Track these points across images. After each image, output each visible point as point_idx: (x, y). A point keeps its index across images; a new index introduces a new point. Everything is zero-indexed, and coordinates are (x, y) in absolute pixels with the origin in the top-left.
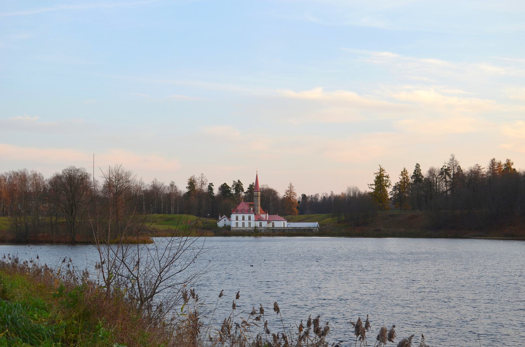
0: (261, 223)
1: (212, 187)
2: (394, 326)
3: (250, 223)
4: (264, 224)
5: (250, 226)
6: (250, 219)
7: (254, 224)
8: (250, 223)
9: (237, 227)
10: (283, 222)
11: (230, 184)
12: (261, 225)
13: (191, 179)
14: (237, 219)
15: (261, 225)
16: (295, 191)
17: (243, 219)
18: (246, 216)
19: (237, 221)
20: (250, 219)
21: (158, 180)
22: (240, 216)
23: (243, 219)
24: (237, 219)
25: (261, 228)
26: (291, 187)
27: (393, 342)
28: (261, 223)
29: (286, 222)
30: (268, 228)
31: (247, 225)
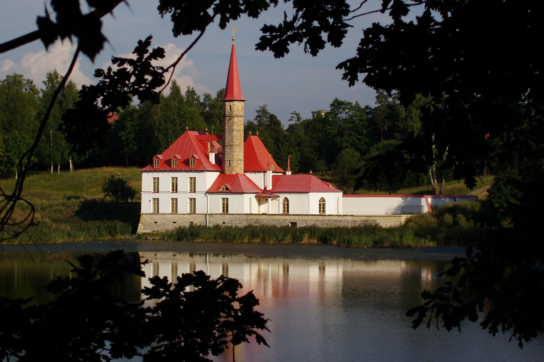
17: (175, 189)
23: (175, 189)
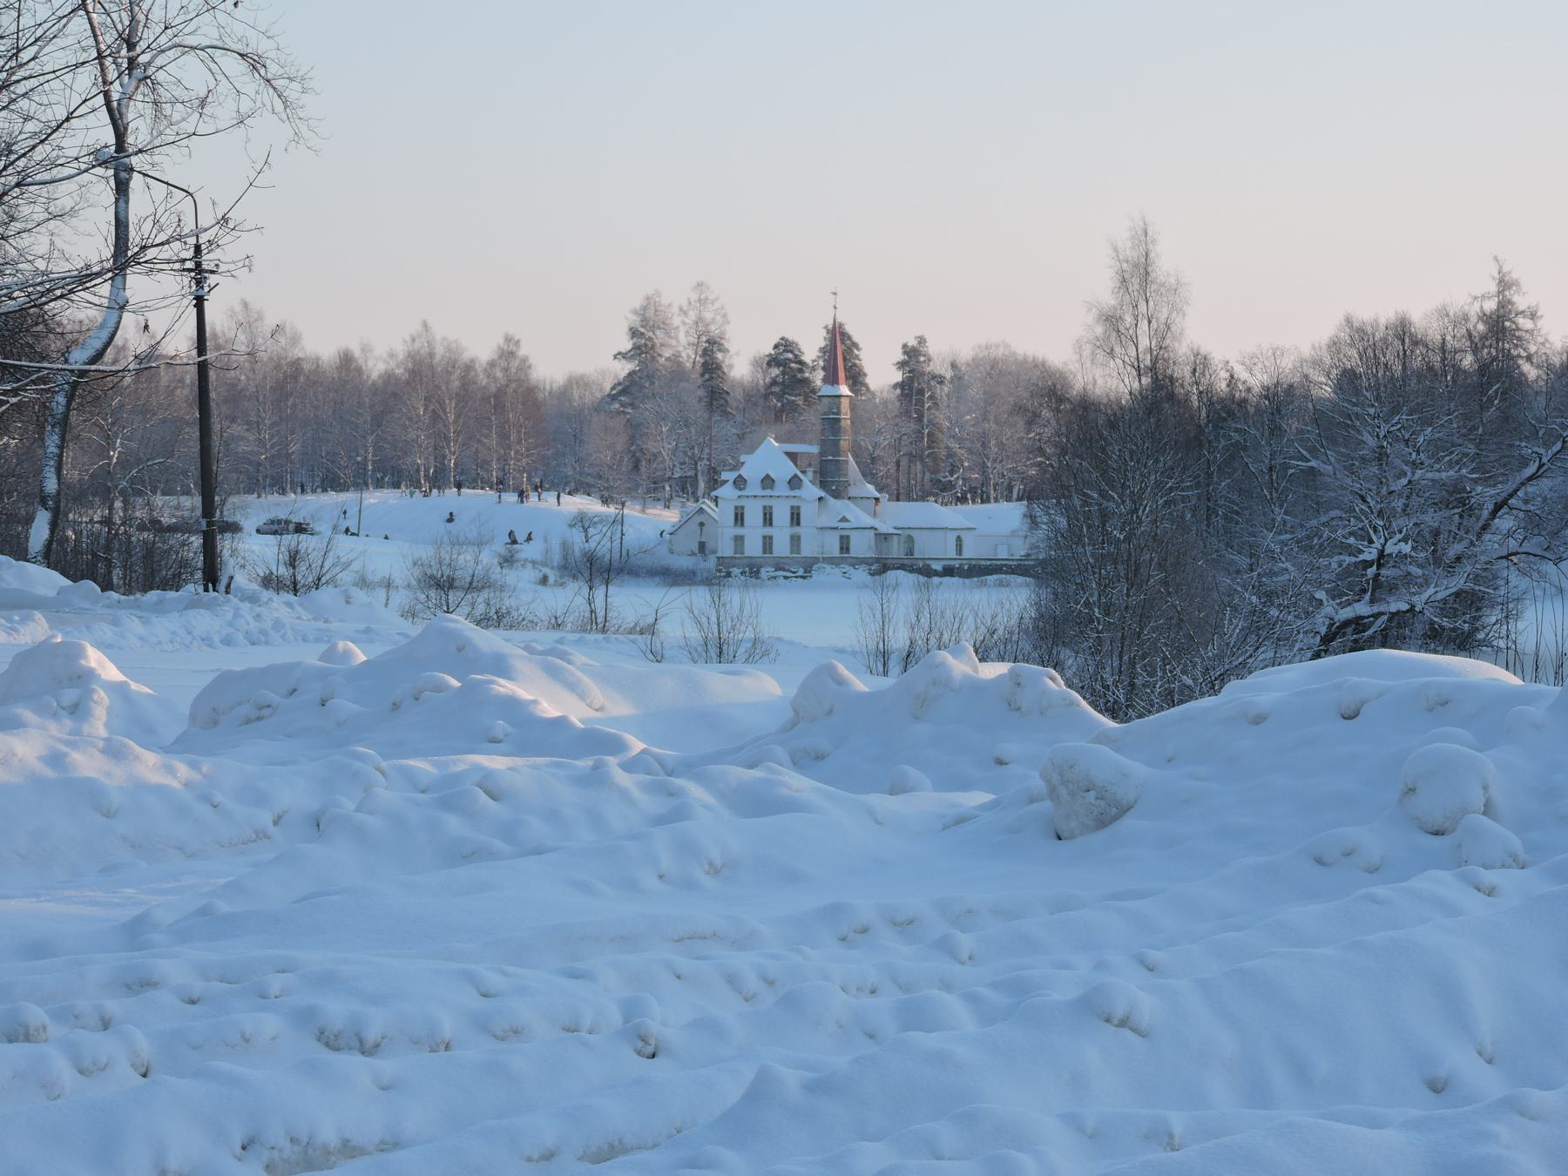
8: (795, 541)
11: (811, 348)
17: (768, 519)
23: (768, 519)
24: (739, 518)
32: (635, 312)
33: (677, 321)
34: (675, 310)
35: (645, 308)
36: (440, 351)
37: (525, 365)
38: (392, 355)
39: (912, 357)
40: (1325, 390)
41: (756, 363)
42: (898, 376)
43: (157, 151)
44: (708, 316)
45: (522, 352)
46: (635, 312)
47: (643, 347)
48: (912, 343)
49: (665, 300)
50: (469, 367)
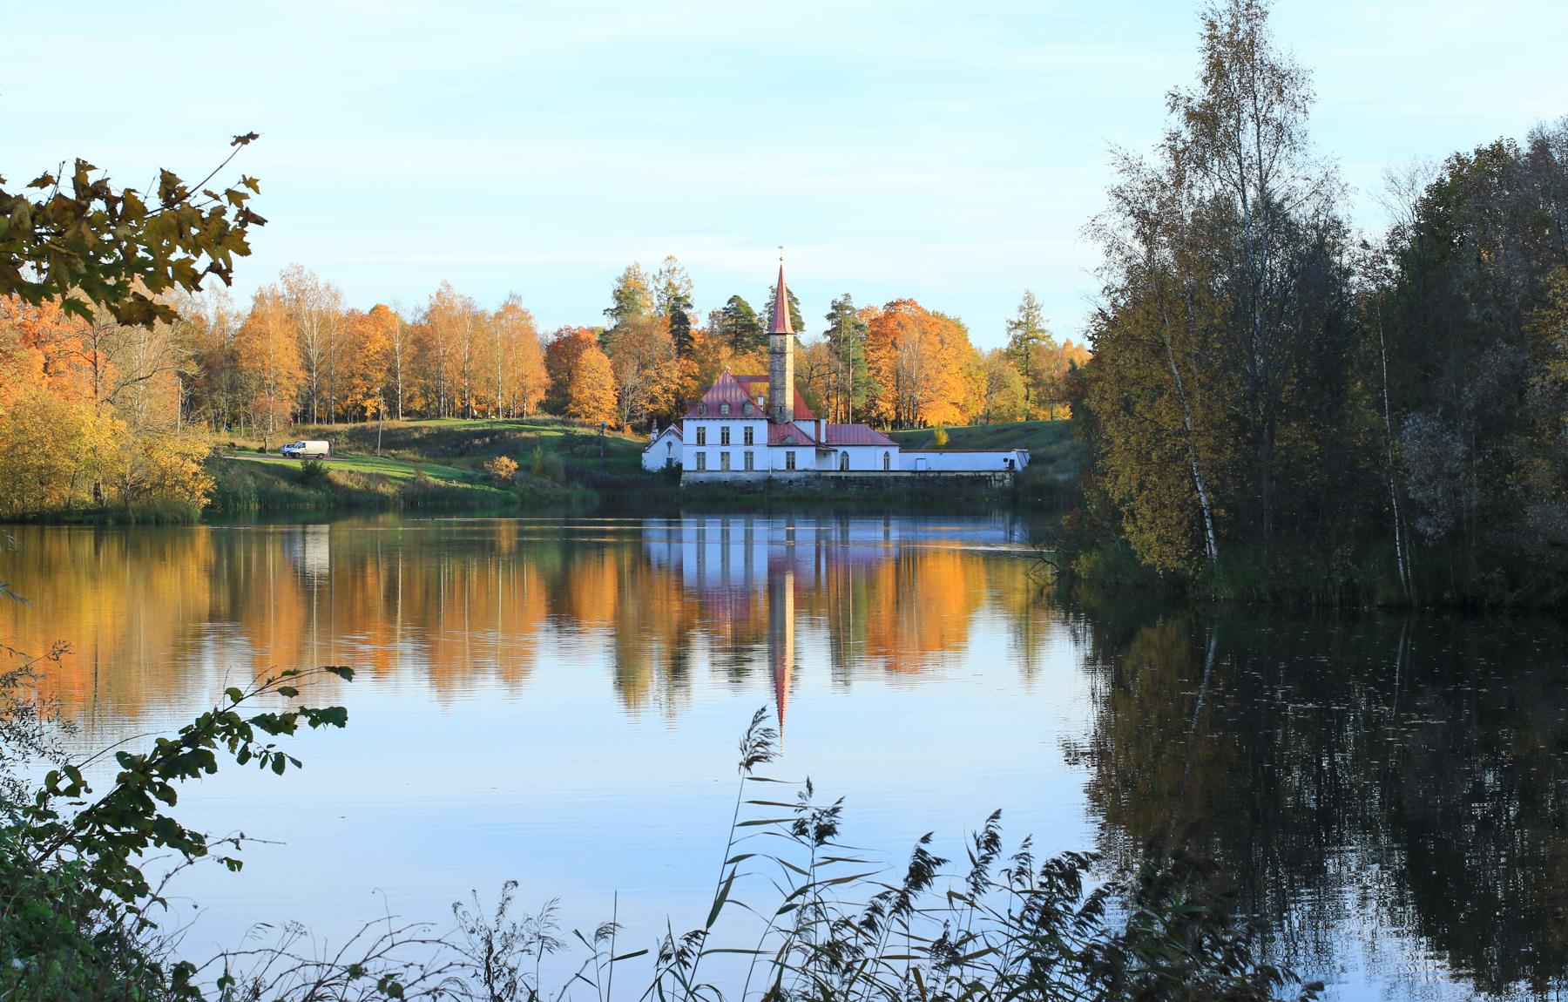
0: (791, 456)
1: (686, 311)
2: (996, 815)
3: (749, 456)
4: (806, 459)
5: (701, 467)
6: (749, 438)
7: (770, 460)
8: (749, 456)
9: (701, 467)
10: (884, 450)
12: (791, 465)
13: (625, 280)
14: (701, 439)
15: (791, 465)
16: (1044, 326)
17: (725, 439)
18: (737, 429)
19: (725, 449)
20: (749, 438)
21: (457, 290)
22: (713, 429)
23: (725, 439)
24: (701, 439)
25: (793, 475)
26: (1030, 308)
27: (121, 756)
28: (791, 456)
29: (894, 452)
30: (818, 475)
31: (737, 463)
32: (620, 280)
33: (651, 287)
34: (650, 277)
35: (627, 277)
36: (457, 303)
37: (525, 316)
38: (418, 310)
39: (838, 311)
40: (1525, 147)
41: (713, 316)
42: (828, 326)
43: (978, 961)
44: (676, 283)
45: (524, 306)
46: (620, 280)
47: (625, 299)
48: (840, 299)
49: (642, 271)
50: (477, 318)
